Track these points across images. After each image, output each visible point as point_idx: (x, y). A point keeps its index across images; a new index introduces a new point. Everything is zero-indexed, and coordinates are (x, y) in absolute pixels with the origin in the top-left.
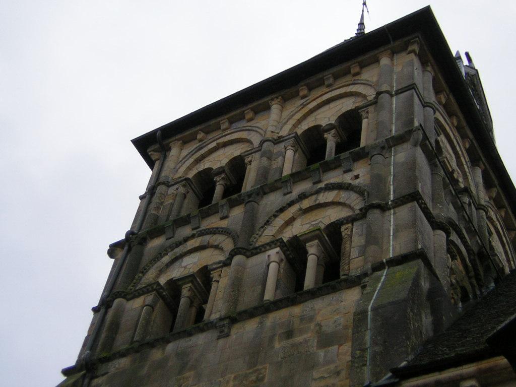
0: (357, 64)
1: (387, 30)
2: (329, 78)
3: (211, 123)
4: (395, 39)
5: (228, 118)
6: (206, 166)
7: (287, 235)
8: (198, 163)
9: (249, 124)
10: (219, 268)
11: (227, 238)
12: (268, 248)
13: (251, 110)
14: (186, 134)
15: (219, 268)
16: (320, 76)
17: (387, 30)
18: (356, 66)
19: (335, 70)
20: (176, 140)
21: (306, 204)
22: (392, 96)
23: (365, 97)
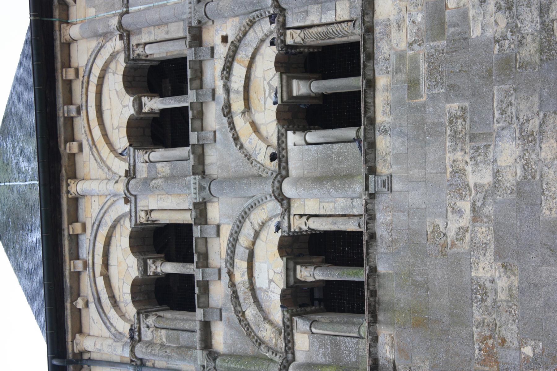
0: (64, 70)
1: (38, 18)
2: (68, 108)
3: (68, 284)
4: (52, 17)
5: (70, 260)
6: (127, 289)
7: (277, 314)
8: (118, 306)
9: (89, 230)
10: (289, 218)
11: (249, 219)
12: (284, 145)
13: (71, 224)
14: (68, 284)
15: (289, 218)
16: (61, 121)
17: (38, 18)
18: (66, 72)
19: (60, 100)
20: (72, 342)
21: (238, 105)
22: (127, 12)
23: (113, 56)
